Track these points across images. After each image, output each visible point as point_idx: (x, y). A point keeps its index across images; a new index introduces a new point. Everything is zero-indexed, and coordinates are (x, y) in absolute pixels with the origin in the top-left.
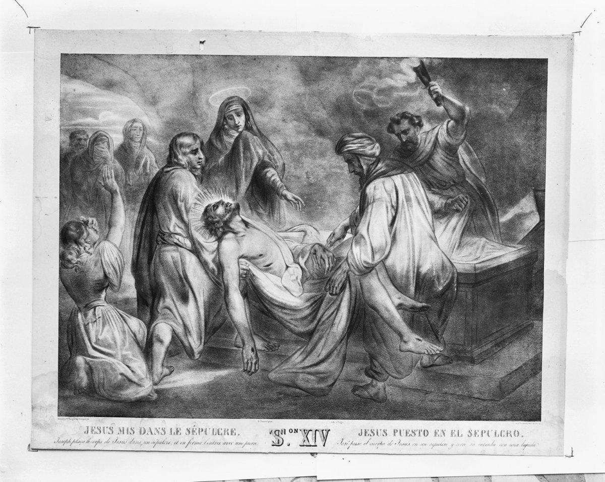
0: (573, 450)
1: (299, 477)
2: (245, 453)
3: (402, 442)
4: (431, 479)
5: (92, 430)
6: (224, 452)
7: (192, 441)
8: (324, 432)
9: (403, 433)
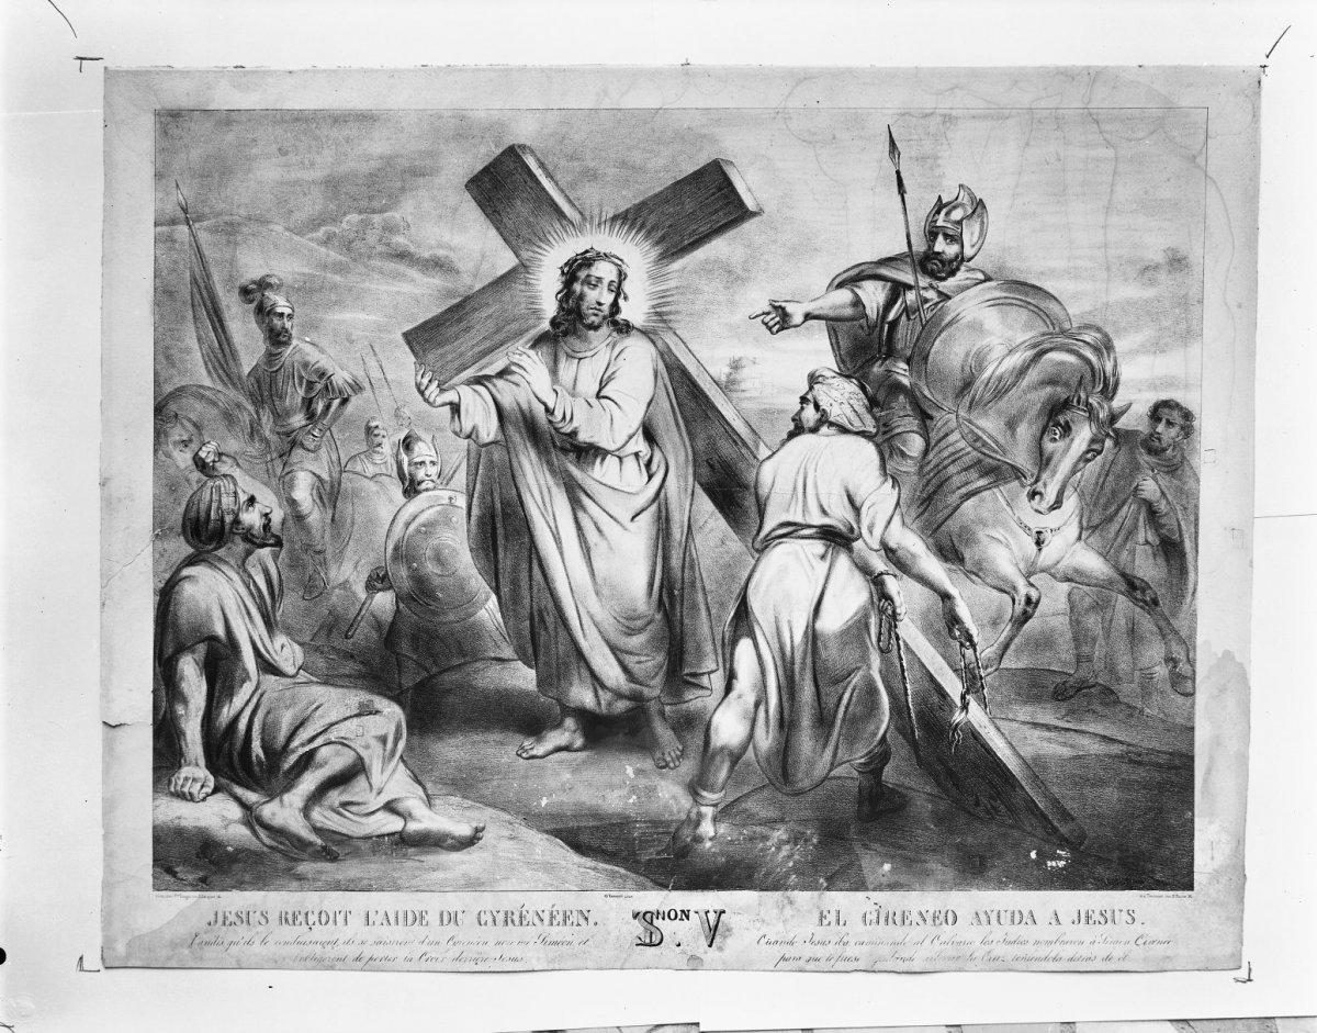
2: (1105, 972)
3: (816, 939)
5: (1088, 917)
6: (1087, 972)
7: (1061, 939)
9: (1006, 919)
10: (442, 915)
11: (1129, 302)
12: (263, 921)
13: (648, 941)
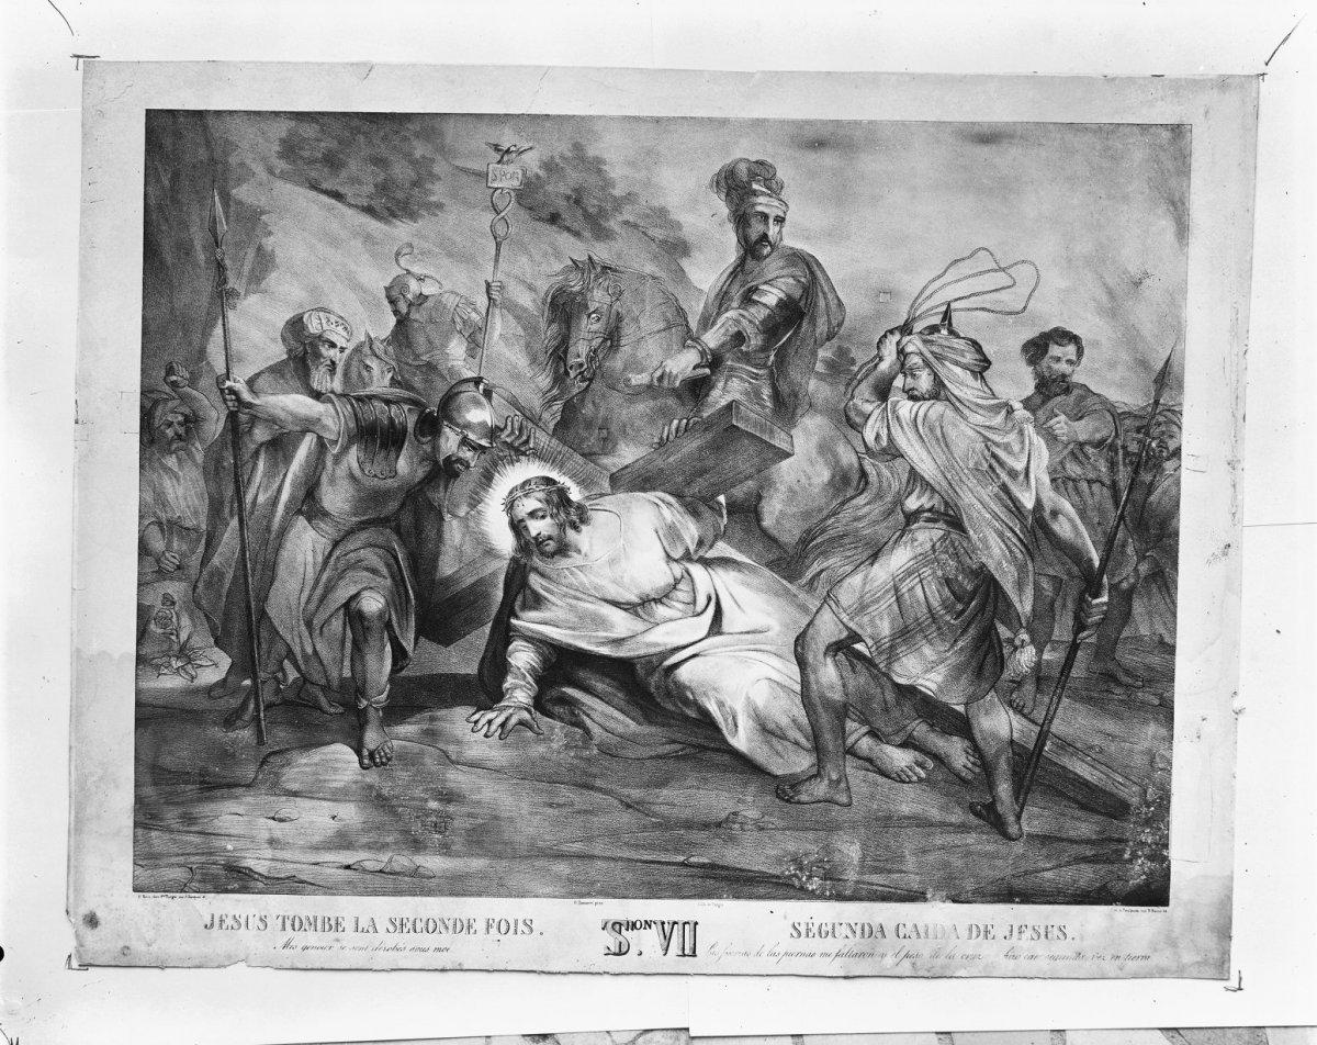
0: (1242, 975)
1: (652, 1030)
4: (935, 1037)
6: (732, 975)
8: (666, 926)
10: (970, 930)
11: (700, 449)
12: (262, 926)
13: (617, 951)
